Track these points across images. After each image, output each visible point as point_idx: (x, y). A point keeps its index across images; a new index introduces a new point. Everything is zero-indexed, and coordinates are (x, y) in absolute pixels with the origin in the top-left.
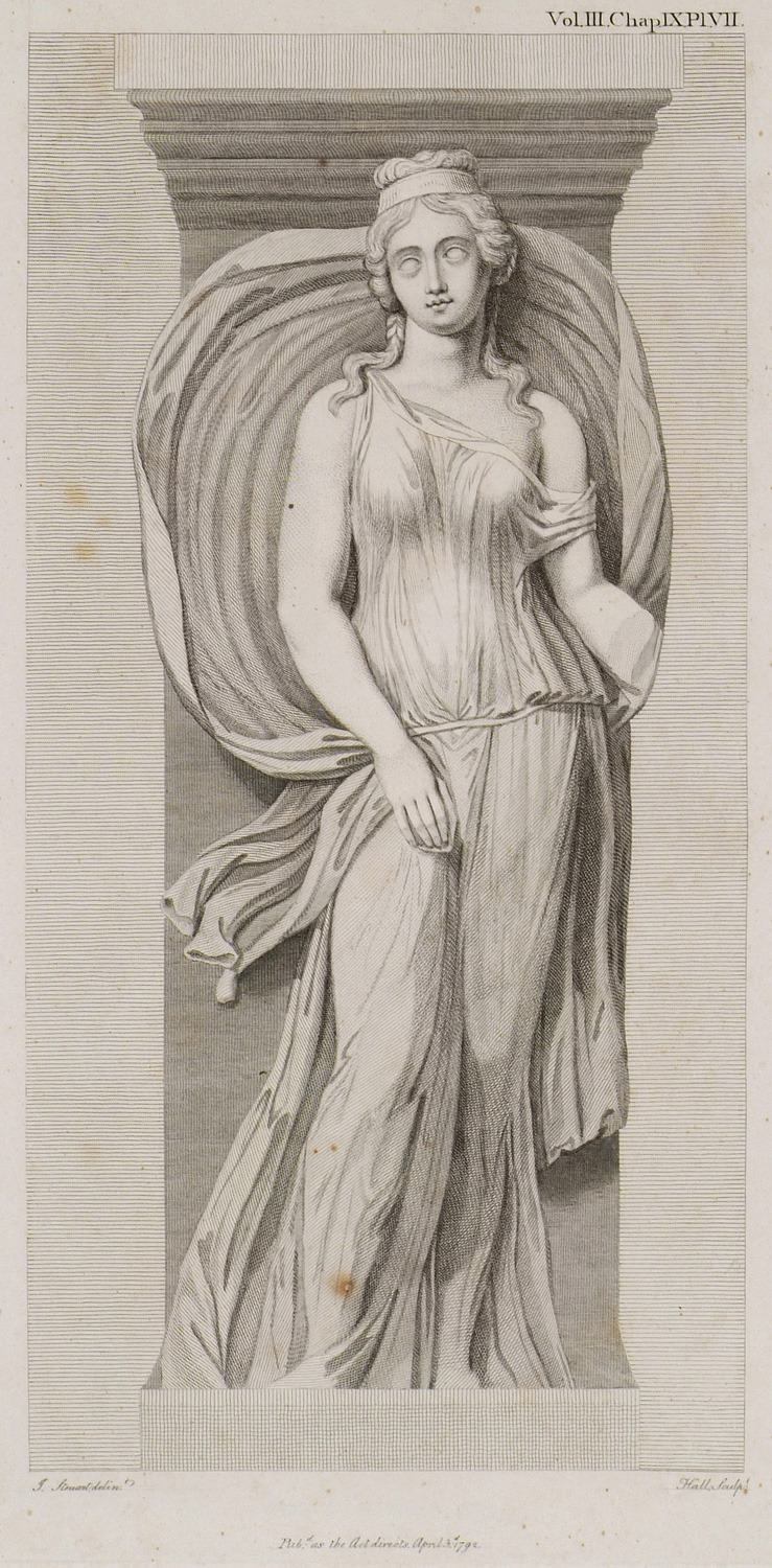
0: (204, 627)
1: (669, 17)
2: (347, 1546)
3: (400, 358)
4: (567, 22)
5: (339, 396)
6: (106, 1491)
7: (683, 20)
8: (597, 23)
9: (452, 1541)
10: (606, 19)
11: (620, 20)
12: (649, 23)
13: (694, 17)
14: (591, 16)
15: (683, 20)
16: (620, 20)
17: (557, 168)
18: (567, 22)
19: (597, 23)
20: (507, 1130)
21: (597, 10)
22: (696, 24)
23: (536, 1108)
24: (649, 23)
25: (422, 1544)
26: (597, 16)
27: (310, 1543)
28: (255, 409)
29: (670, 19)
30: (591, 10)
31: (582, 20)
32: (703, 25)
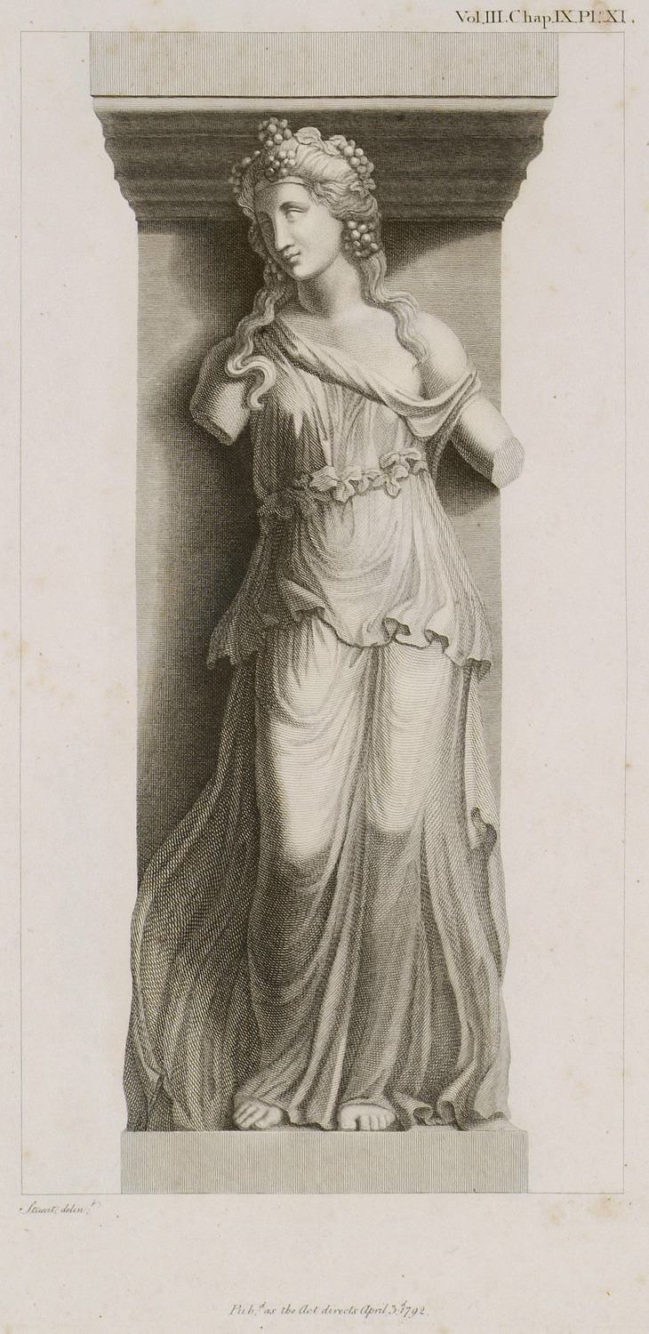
2: (297, 1311)
4: (471, 19)
6: (73, 1213)
7: (575, 16)
9: (399, 1307)
10: (505, 16)
11: (518, 17)
12: (542, 19)
13: (585, 14)
14: (497, 19)
15: (575, 16)
16: (518, 17)
17: (195, 179)
18: (471, 19)
22: (587, 20)
24: (542, 19)
25: (368, 1311)
27: (263, 1310)
28: (316, 1081)
29: (561, 16)
31: (483, 18)
32: (593, 21)
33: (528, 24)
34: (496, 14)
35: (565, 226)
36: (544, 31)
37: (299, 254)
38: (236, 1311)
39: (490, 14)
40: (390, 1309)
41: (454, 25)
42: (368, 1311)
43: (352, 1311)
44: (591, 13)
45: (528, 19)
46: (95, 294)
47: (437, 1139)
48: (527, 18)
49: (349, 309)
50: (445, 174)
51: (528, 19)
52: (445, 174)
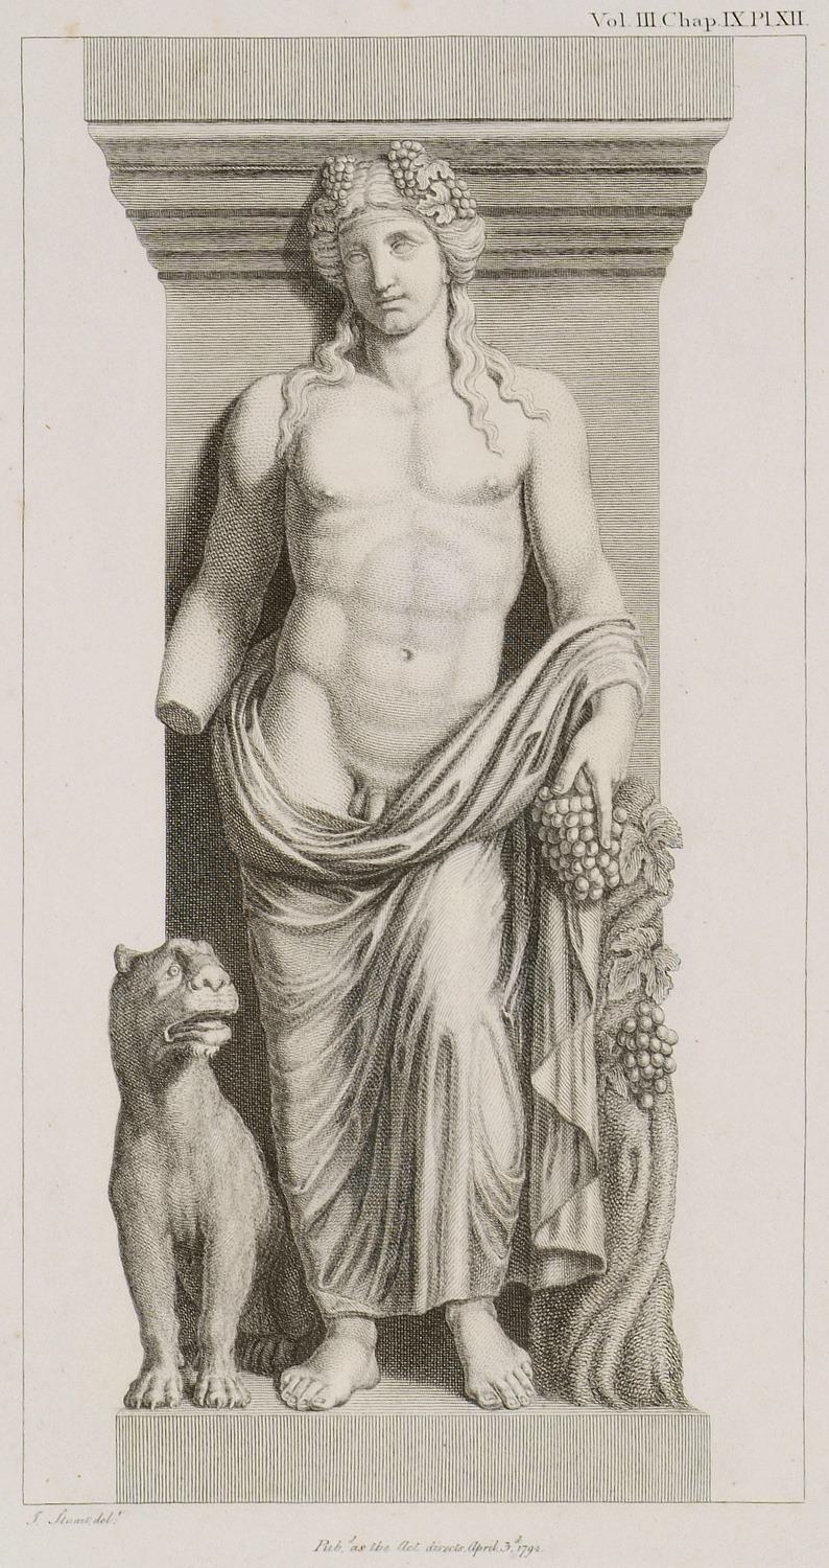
0: (227, 1360)
1: (730, 16)
3: (507, 401)
4: (612, 23)
5: (451, 1037)
8: (650, 23)
10: (658, 20)
12: (704, 22)
13: (758, 16)
14: (643, 17)
15: (746, 19)
16: (673, 20)
19: (650, 23)
20: (531, 771)
21: (649, 11)
22: (761, 22)
23: (572, 990)
26: (649, 16)
29: (788, 19)
30: (642, 11)
31: (631, 19)
32: (754, 25)
33: (685, 28)
34: (643, 23)
35: (736, 277)
36: (708, 34)
37: (404, 296)
38: (322, 1548)
39: (643, 17)
40: (499, 1546)
41: (587, 28)
42: (477, 1548)
43: (458, 1549)
44: (765, 15)
45: (685, 23)
46: (106, 373)
47: (587, 1422)
48: (683, 21)
49: (417, 357)
50: (585, 211)
51: (685, 23)
52: (585, 211)
